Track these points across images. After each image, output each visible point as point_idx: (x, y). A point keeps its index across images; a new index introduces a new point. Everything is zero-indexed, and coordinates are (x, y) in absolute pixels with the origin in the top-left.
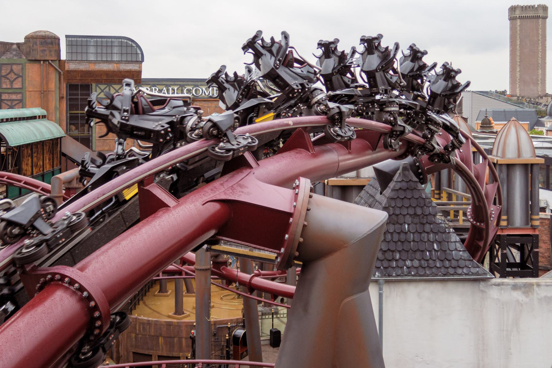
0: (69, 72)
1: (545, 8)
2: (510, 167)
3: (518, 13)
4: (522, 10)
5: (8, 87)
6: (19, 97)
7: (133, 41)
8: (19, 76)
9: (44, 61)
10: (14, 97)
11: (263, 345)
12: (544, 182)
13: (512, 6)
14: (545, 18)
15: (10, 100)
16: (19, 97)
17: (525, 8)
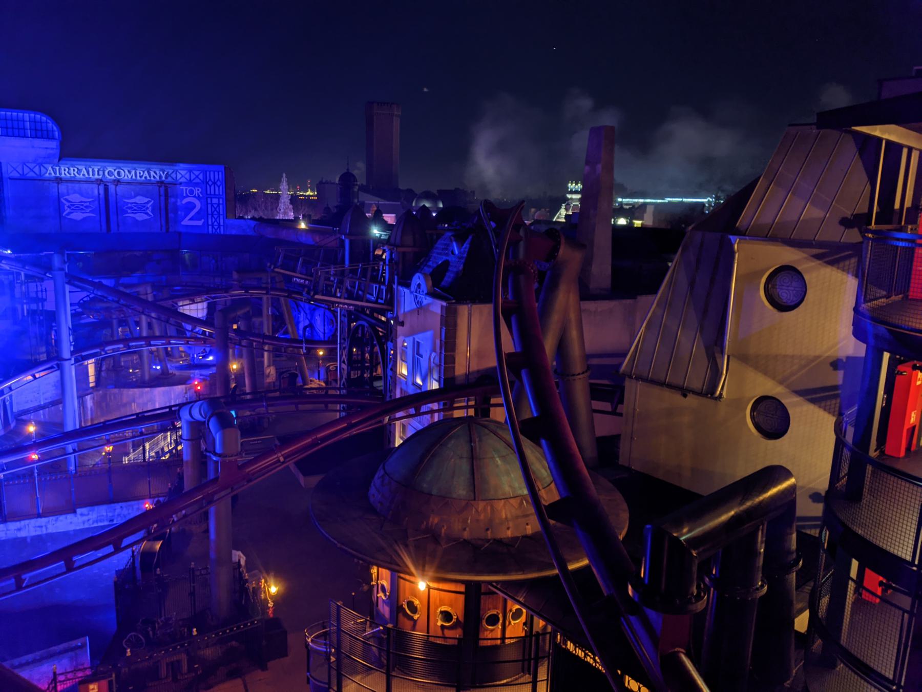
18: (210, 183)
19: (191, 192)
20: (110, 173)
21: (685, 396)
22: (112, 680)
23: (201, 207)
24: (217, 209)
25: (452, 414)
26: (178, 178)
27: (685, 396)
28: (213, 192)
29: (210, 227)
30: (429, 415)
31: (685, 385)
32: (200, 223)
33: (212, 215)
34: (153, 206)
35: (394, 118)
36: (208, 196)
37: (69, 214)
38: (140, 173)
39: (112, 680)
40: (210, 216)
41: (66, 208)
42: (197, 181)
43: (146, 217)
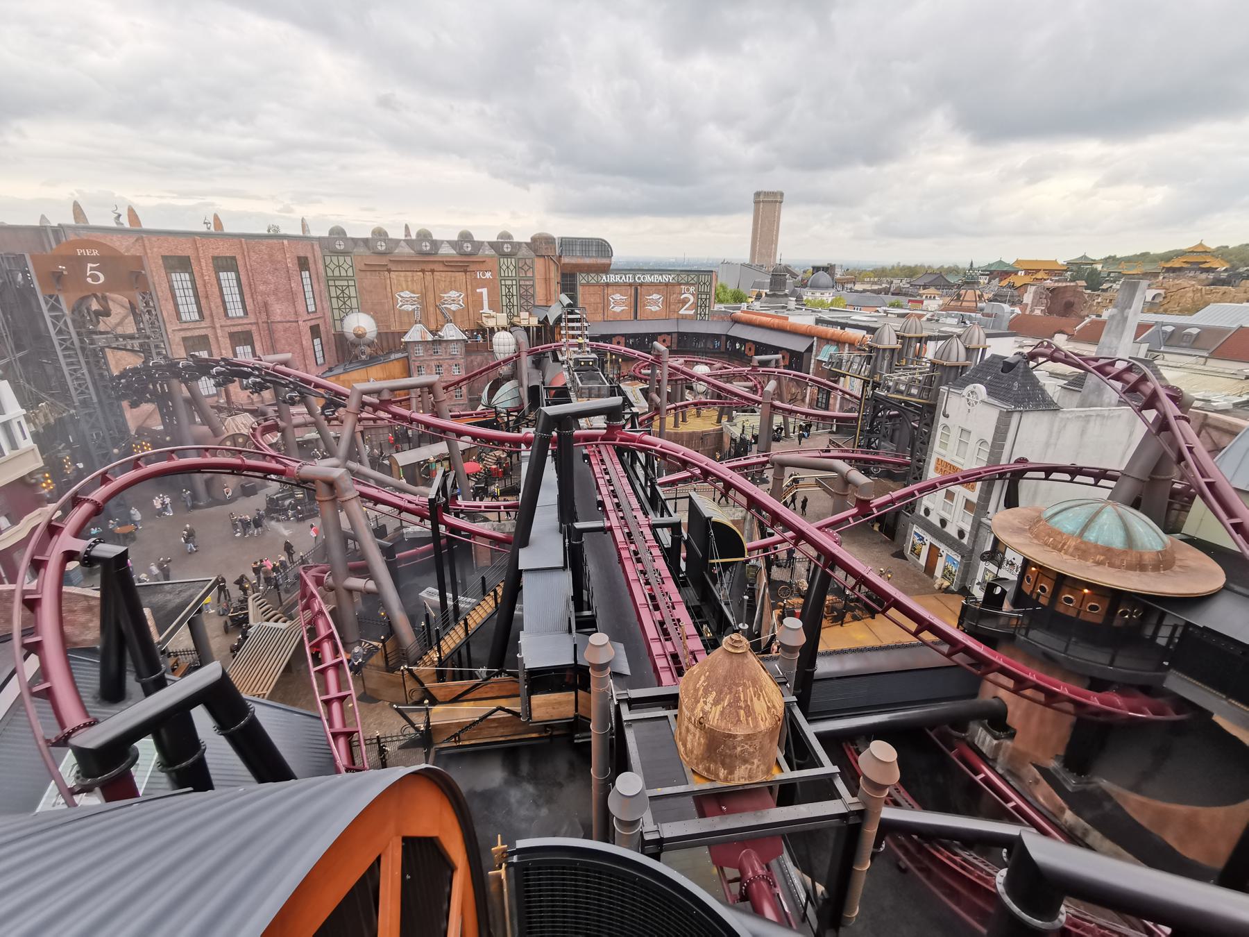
1: (782, 194)
2: (884, 350)
3: (761, 198)
6: (531, 283)
7: (606, 242)
8: (530, 268)
9: (548, 256)
10: (528, 283)
11: (1145, 395)
13: (942, 267)
14: (781, 202)
17: (767, 194)
19: (688, 290)
20: (639, 278)
21: (679, 620)
22: (310, 385)
27: (679, 620)
30: (192, 647)
31: (327, 498)
32: (692, 312)
33: (701, 306)
34: (663, 301)
35: (570, 696)
39: (310, 385)
42: (692, 282)
43: (658, 308)
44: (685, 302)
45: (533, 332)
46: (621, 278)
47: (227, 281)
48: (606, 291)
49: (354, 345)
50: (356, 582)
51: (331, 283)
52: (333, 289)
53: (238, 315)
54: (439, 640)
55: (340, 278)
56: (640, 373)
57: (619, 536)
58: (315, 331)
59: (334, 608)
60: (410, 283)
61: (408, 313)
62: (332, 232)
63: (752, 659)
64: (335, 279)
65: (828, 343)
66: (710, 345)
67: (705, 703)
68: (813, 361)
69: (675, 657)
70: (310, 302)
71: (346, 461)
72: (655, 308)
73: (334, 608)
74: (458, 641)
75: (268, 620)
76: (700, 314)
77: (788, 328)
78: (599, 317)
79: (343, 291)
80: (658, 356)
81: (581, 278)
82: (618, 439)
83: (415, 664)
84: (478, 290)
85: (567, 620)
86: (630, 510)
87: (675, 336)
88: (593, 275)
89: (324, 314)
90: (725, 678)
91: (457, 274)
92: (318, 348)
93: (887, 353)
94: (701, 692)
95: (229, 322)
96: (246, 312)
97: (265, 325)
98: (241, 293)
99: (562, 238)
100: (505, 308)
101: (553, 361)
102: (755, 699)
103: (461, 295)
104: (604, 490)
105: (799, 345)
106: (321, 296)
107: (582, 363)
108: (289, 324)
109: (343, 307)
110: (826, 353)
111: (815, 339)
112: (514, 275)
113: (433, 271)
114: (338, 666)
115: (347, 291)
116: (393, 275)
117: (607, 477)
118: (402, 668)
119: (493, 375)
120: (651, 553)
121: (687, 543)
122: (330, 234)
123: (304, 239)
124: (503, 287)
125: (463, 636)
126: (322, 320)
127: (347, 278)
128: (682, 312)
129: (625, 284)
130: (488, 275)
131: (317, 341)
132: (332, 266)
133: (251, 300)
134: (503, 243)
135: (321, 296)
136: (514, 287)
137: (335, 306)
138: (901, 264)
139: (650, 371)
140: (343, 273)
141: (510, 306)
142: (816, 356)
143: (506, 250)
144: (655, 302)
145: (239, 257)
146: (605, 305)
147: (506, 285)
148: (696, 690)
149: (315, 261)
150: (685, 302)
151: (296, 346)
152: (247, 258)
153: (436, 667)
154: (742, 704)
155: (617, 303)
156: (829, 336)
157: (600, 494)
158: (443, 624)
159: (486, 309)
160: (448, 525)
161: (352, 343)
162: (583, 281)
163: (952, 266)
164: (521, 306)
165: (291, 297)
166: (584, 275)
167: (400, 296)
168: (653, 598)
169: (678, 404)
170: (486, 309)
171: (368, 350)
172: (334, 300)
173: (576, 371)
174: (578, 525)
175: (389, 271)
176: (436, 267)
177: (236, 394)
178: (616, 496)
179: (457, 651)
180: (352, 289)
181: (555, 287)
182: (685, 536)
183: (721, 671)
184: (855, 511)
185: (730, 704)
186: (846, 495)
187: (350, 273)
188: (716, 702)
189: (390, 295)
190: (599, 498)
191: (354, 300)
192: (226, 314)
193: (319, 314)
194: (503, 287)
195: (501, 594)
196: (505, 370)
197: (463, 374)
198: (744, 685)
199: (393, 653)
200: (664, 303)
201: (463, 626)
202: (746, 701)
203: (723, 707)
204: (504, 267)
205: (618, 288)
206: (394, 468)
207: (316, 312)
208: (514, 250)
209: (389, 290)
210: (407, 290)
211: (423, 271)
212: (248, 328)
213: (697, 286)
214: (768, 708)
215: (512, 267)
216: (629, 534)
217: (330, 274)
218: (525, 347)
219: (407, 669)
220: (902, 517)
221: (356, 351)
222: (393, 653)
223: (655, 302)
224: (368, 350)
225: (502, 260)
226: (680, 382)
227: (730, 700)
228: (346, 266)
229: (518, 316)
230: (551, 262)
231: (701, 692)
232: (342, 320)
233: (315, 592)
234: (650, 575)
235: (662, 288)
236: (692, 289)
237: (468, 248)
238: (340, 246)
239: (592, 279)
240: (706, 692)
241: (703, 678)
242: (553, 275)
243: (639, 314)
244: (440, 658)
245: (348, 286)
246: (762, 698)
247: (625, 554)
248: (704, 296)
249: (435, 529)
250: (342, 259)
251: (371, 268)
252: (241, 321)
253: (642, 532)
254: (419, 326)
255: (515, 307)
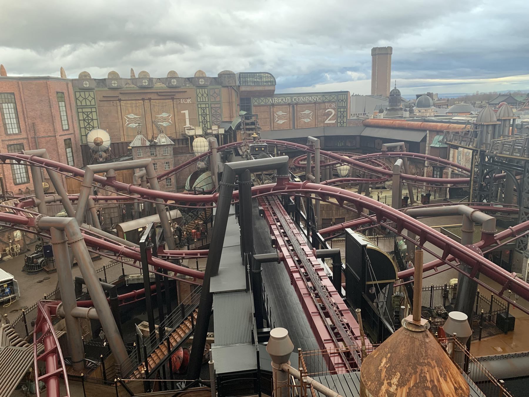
0: (242, 92)
2: (488, 126)
3: (377, 52)
4: (379, 50)
5: (214, 100)
6: (219, 106)
10: (217, 106)
12: (3, 244)
15: (215, 107)
16: (219, 106)
18: (340, 101)
19: (331, 106)
23: (335, 114)
24: (343, 114)
25: (314, 204)
26: (265, 100)
28: (341, 106)
29: (339, 124)
32: (334, 122)
36: (94, 106)
37: (128, 124)
38: (308, 98)
40: (339, 118)
41: (127, 121)
42: (333, 100)
43: (309, 120)
44: (329, 114)
45: (221, 138)
46: (282, 100)
47: (11, 117)
48: (272, 110)
49: (95, 152)
50: (83, 311)
51: (80, 110)
52: (81, 114)
53: (14, 132)
54: (146, 358)
55: (86, 106)
56: (299, 164)
57: (290, 263)
58: (68, 143)
59: (65, 333)
60: (134, 108)
61: (132, 129)
62: (81, 75)
63: (431, 339)
64: (83, 107)
65: (438, 134)
66: (349, 144)
67: (390, 384)
68: (427, 148)
69: (348, 354)
70: (65, 123)
71: (81, 224)
72: (307, 120)
73: (64, 335)
74: (161, 357)
75: (15, 345)
76: (340, 123)
77: (407, 127)
78: (267, 128)
79: (88, 116)
80: (311, 146)
81: (254, 101)
82: (287, 188)
83: (127, 377)
84: (182, 112)
85: (251, 334)
86: (298, 245)
87: (323, 139)
88: (262, 99)
89: (74, 131)
90: (408, 358)
91: (167, 101)
92: (70, 155)
93: (490, 128)
94: (383, 374)
95: (8, 138)
96: (20, 131)
97: (33, 139)
98: (17, 118)
99: (240, 73)
100: (201, 123)
101: (236, 155)
102: (442, 380)
103: (170, 115)
104: (276, 232)
105: (416, 137)
106: (72, 119)
107: (257, 149)
108: (49, 138)
109: (88, 126)
110: (436, 142)
111: (428, 132)
112: (207, 100)
113: (150, 99)
114: (59, 376)
115: (90, 116)
116: (123, 103)
117: (279, 224)
118: (115, 380)
119: (193, 169)
120: (318, 274)
121: (346, 271)
122: (79, 77)
123: (62, 80)
124: (200, 109)
125: (166, 353)
126: (73, 135)
127: (91, 107)
128: (327, 122)
129: (285, 104)
130: (189, 101)
131: (69, 150)
132: (81, 99)
133: (24, 122)
134: (199, 78)
135: (72, 119)
136: (207, 109)
137: (82, 126)
138: (480, 92)
139: (306, 162)
140: (88, 103)
141: (204, 122)
142: (429, 144)
143: (201, 83)
144: (307, 116)
145: (17, 93)
146: (272, 120)
147: (201, 108)
148: (379, 372)
149: (69, 95)
150: (329, 114)
151: (54, 153)
152: (22, 93)
153: (144, 378)
154: (429, 384)
155: (280, 118)
156: (438, 129)
157: (274, 235)
158: (152, 342)
159: (188, 125)
160: (156, 266)
161: (93, 151)
162: (256, 103)
163: (516, 91)
164: (212, 122)
165: (52, 119)
166: (256, 99)
167: (128, 117)
168: (324, 308)
169: (328, 181)
170: (188, 125)
171: (104, 155)
172: (82, 122)
173: (252, 155)
174: (257, 256)
175: (120, 100)
176: (152, 96)
177: (10, 187)
178: (286, 236)
179: (162, 364)
180: (94, 114)
181: (236, 108)
182: (344, 266)
183: (402, 351)
184: (482, 243)
185: (416, 385)
186: (472, 232)
187: (93, 103)
188: (401, 384)
189: (120, 117)
190: (273, 238)
191: (95, 122)
192: (6, 133)
193: (71, 131)
194: (200, 109)
195: (196, 317)
196: (201, 165)
197: (172, 168)
198: (429, 364)
199: (109, 370)
200: (314, 117)
201: (166, 344)
202: (432, 381)
203: (409, 388)
204: (200, 95)
205: (280, 107)
206: (120, 233)
207: (68, 130)
208: (207, 83)
209: (120, 113)
210: (132, 113)
211: (143, 100)
212: (21, 141)
213: (337, 103)
214: (456, 389)
215: (205, 95)
216: (299, 261)
217: (79, 104)
218: (216, 145)
219: (120, 381)
220: (516, 254)
221: (96, 156)
222: (109, 370)
223: (307, 116)
224: (104, 155)
225: (198, 90)
226: (328, 167)
227: (416, 380)
228: (90, 98)
229: (211, 129)
230: (233, 91)
231: (383, 374)
232: (86, 135)
233: (47, 317)
234: (319, 290)
235: (312, 105)
236: (333, 105)
237: (174, 82)
238: (86, 85)
239: (263, 101)
240: (390, 376)
241: (384, 361)
242: (234, 100)
243: (296, 125)
244: (147, 371)
245: (91, 112)
246: (448, 380)
247: (296, 275)
248: (342, 110)
249: (146, 271)
250: (87, 94)
251: (107, 99)
252: (16, 137)
253: (309, 260)
254: (139, 137)
255: (208, 123)
